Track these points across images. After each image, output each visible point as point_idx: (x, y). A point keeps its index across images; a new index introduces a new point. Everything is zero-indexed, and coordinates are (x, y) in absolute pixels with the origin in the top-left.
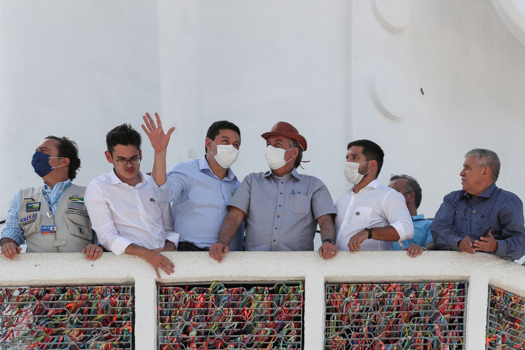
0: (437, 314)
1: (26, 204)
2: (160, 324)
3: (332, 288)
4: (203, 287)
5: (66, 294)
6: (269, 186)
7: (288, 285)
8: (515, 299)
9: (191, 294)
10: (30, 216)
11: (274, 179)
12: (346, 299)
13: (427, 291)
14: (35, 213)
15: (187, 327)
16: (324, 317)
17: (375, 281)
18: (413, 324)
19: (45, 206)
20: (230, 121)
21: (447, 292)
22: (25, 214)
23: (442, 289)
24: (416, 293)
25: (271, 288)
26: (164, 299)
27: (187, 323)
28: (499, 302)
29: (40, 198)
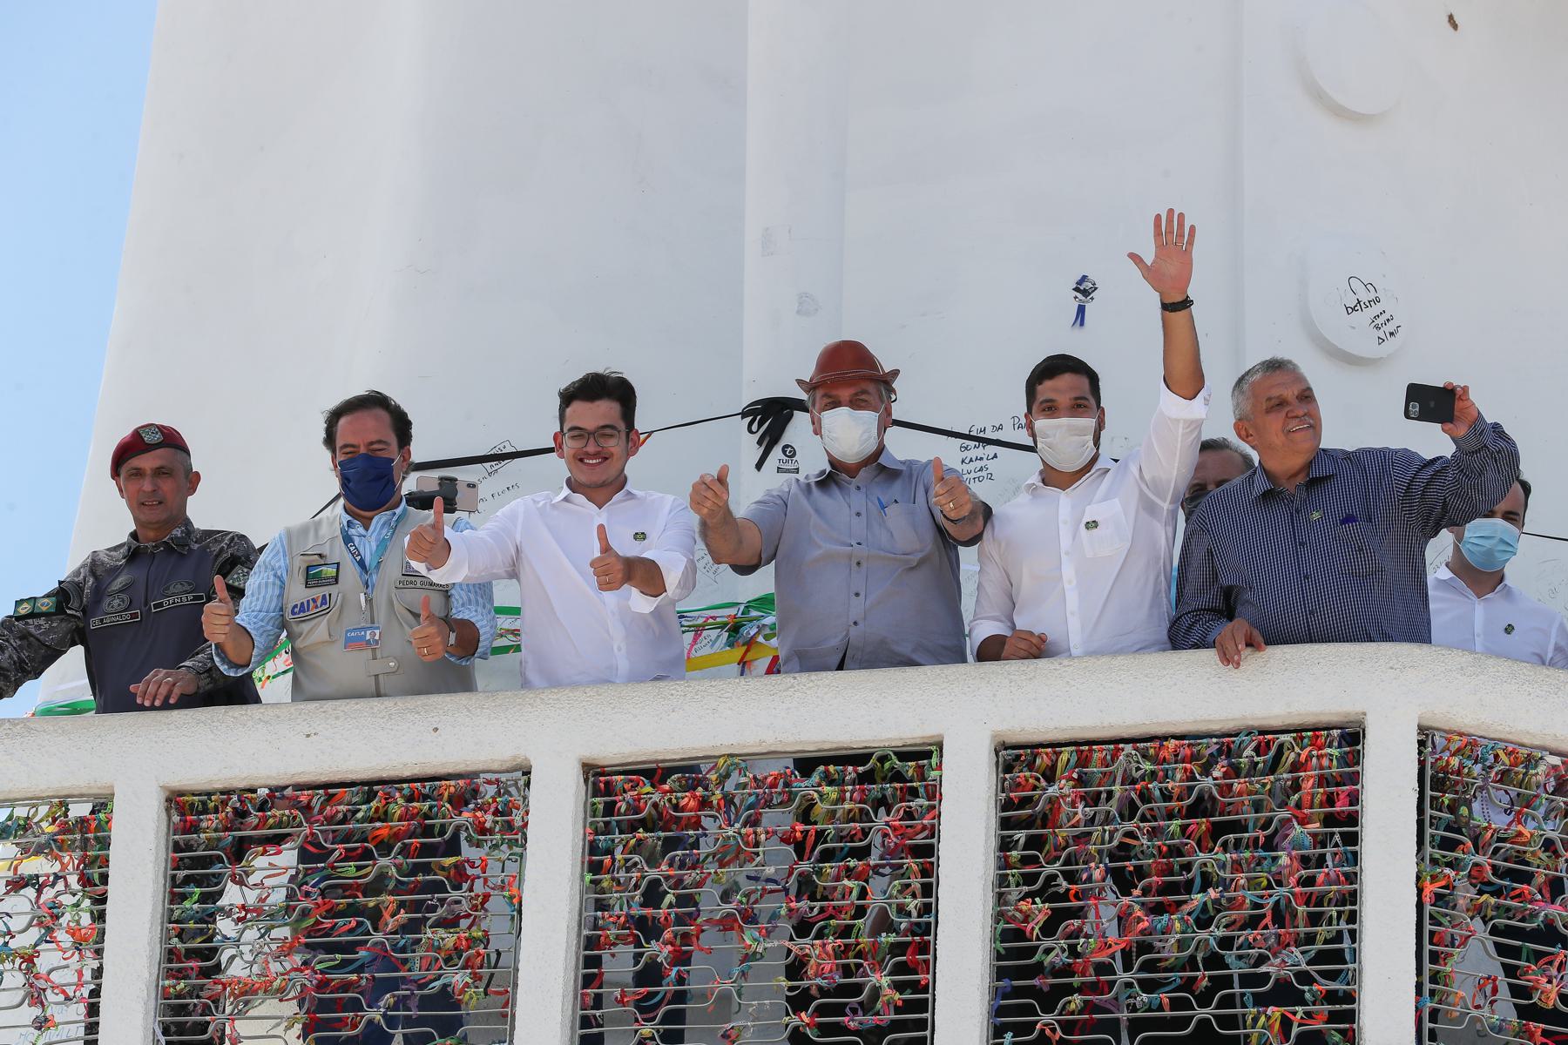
0: (1285, 823)
1: (304, 566)
2: (589, 877)
3: (1017, 759)
4: (688, 772)
5: (374, 804)
6: (832, 503)
7: (904, 756)
8: (1509, 754)
9: (665, 792)
10: (314, 600)
11: (837, 483)
12: (1050, 790)
13: (1256, 759)
14: (325, 590)
15: (654, 884)
16: (993, 843)
17: (1125, 735)
18: (1221, 856)
19: (350, 572)
20: (415, 431)
21: (1309, 757)
22: (298, 593)
23: (1297, 749)
24: (1231, 765)
25: (861, 769)
26: (601, 807)
27: (653, 874)
28: (1459, 773)
29: (339, 552)
